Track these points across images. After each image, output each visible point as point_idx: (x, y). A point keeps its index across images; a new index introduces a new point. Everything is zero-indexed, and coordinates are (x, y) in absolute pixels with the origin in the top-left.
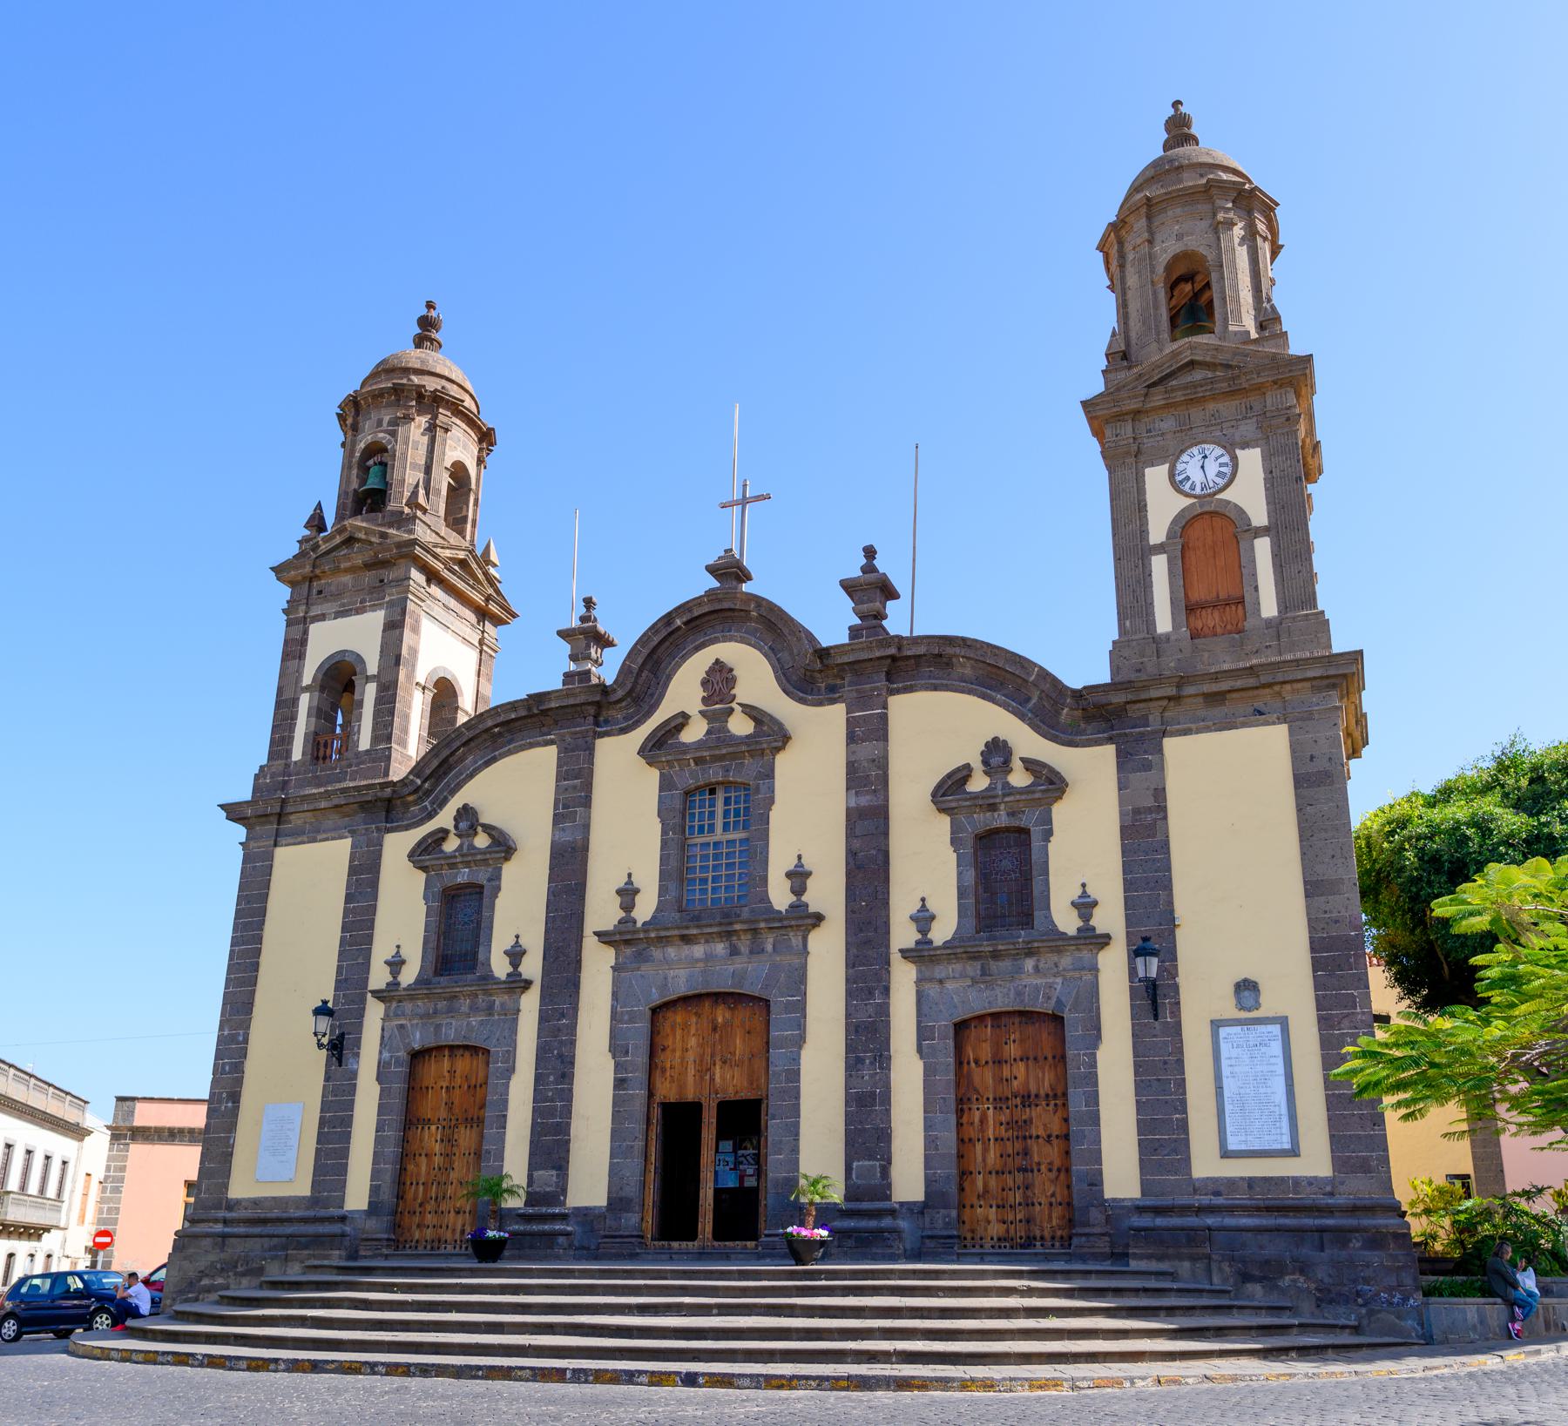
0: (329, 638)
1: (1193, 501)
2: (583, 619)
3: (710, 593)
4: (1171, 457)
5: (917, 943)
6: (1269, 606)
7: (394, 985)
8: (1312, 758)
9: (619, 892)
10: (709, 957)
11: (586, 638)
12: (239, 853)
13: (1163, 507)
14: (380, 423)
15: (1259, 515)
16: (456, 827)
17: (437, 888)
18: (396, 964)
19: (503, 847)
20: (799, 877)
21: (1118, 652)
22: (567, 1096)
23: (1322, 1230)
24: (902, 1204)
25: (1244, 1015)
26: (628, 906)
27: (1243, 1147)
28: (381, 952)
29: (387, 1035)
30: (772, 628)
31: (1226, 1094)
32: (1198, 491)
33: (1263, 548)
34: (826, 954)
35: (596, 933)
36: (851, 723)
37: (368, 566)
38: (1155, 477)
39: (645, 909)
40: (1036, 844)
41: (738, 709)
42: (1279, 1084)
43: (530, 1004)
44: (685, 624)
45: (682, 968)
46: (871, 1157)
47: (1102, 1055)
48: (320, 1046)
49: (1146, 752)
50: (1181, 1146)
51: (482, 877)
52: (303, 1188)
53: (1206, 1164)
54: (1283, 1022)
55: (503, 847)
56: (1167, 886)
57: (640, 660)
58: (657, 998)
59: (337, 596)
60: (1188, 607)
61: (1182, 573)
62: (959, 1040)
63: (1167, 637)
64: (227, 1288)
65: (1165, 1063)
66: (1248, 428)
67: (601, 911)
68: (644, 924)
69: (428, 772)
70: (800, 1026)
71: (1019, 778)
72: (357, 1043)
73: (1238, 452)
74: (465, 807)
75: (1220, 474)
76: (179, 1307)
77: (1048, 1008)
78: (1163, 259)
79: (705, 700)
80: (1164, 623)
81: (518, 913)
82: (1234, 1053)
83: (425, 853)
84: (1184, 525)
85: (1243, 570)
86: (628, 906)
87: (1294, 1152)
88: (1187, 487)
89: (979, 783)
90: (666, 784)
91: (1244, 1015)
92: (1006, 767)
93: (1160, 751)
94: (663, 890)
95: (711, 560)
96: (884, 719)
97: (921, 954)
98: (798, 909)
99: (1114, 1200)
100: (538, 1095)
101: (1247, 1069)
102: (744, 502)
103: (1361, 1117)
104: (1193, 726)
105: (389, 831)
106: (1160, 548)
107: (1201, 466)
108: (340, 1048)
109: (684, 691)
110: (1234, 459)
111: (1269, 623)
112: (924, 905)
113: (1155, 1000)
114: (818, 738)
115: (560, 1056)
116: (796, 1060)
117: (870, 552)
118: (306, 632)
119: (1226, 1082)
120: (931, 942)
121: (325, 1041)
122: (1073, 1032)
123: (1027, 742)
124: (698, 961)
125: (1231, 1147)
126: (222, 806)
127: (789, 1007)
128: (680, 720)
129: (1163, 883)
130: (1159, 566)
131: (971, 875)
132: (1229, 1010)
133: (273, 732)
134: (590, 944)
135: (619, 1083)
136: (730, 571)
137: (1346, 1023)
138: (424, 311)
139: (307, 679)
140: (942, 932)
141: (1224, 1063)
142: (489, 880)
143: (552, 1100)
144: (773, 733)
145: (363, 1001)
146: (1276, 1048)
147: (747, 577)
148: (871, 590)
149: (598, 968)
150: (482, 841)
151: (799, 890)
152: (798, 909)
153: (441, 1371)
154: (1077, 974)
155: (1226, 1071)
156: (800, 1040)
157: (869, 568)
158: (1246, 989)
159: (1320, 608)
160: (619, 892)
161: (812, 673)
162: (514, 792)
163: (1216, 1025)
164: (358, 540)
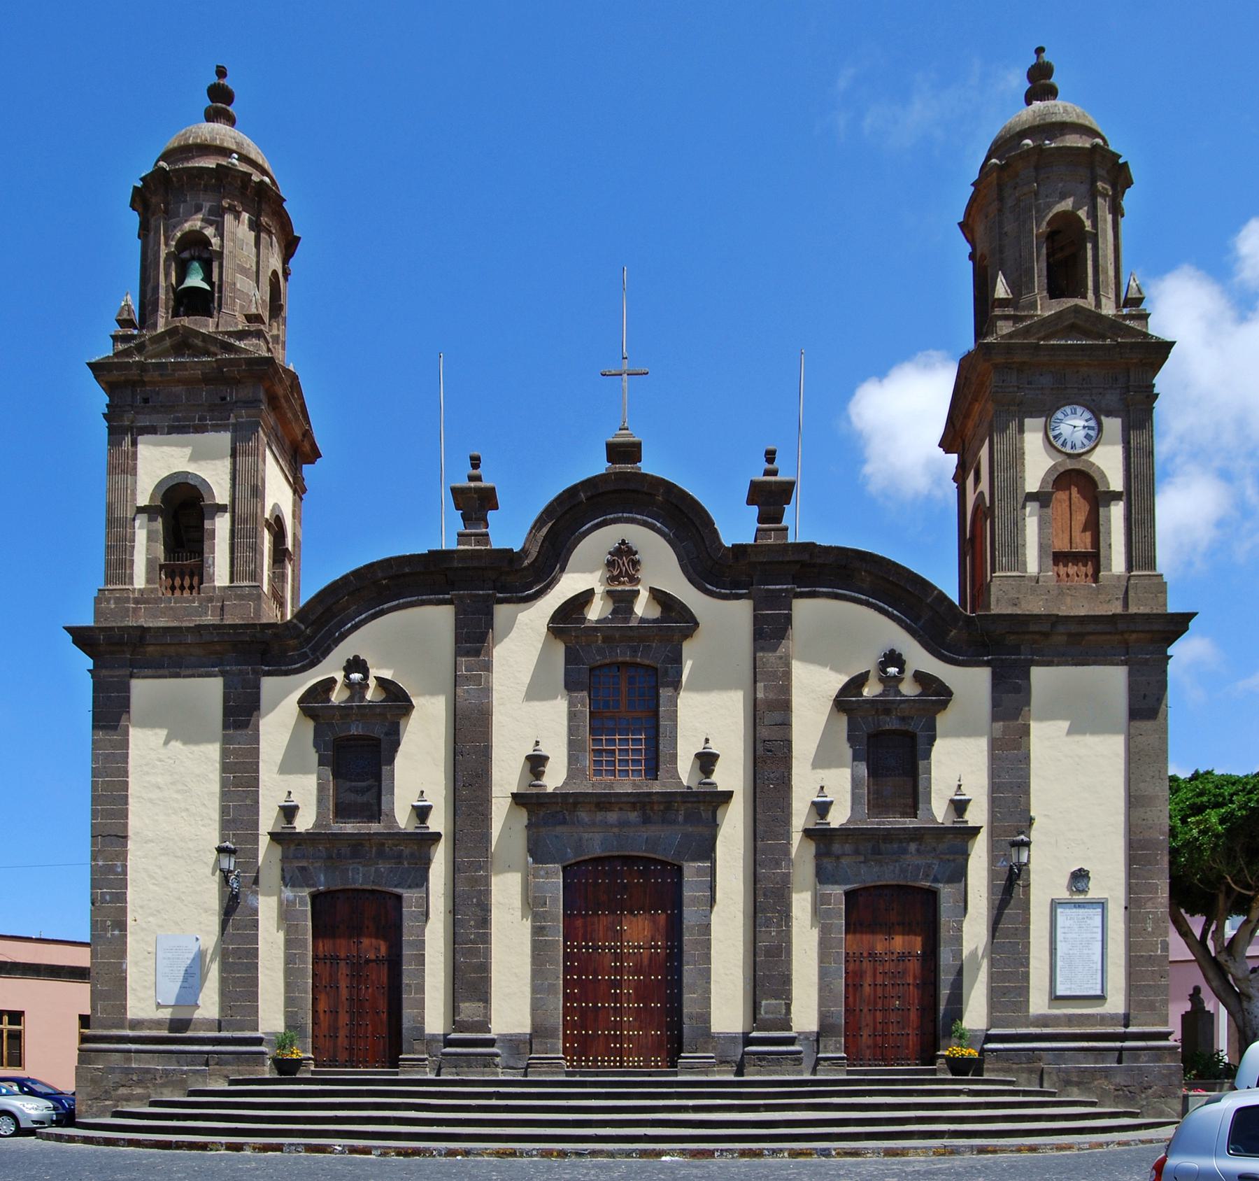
8: (1145, 696)
10: (622, 824)
15: (1116, 482)
17: (329, 738)
19: (397, 702)
23: (1121, 1050)
30: (682, 518)
33: (1117, 512)
51: (378, 731)
54: (1102, 904)
56: (1027, 792)
66: (1112, 398)
67: (506, 776)
71: (908, 689)
73: (1103, 418)
75: (1087, 437)
81: (418, 773)
82: (1068, 923)
88: (1058, 444)
93: (1028, 677)
103: (1153, 972)
104: (1055, 659)
107: (1073, 424)
109: (580, 578)
110: (1100, 424)
113: (1011, 885)
115: (478, 905)
119: (1059, 946)
123: (919, 658)
124: (612, 826)
125: (1059, 993)
129: (1024, 787)
131: (922, 764)
132: (1064, 894)
137: (1149, 904)
138: (214, 79)
142: (387, 734)
146: (1099, 918)
148: (770, 498)
153: (179, 1146)
154: (951, 857)
158: (1080, 877)
159: (1159, 570)
161: (713, 566)
163: (1055, 905)
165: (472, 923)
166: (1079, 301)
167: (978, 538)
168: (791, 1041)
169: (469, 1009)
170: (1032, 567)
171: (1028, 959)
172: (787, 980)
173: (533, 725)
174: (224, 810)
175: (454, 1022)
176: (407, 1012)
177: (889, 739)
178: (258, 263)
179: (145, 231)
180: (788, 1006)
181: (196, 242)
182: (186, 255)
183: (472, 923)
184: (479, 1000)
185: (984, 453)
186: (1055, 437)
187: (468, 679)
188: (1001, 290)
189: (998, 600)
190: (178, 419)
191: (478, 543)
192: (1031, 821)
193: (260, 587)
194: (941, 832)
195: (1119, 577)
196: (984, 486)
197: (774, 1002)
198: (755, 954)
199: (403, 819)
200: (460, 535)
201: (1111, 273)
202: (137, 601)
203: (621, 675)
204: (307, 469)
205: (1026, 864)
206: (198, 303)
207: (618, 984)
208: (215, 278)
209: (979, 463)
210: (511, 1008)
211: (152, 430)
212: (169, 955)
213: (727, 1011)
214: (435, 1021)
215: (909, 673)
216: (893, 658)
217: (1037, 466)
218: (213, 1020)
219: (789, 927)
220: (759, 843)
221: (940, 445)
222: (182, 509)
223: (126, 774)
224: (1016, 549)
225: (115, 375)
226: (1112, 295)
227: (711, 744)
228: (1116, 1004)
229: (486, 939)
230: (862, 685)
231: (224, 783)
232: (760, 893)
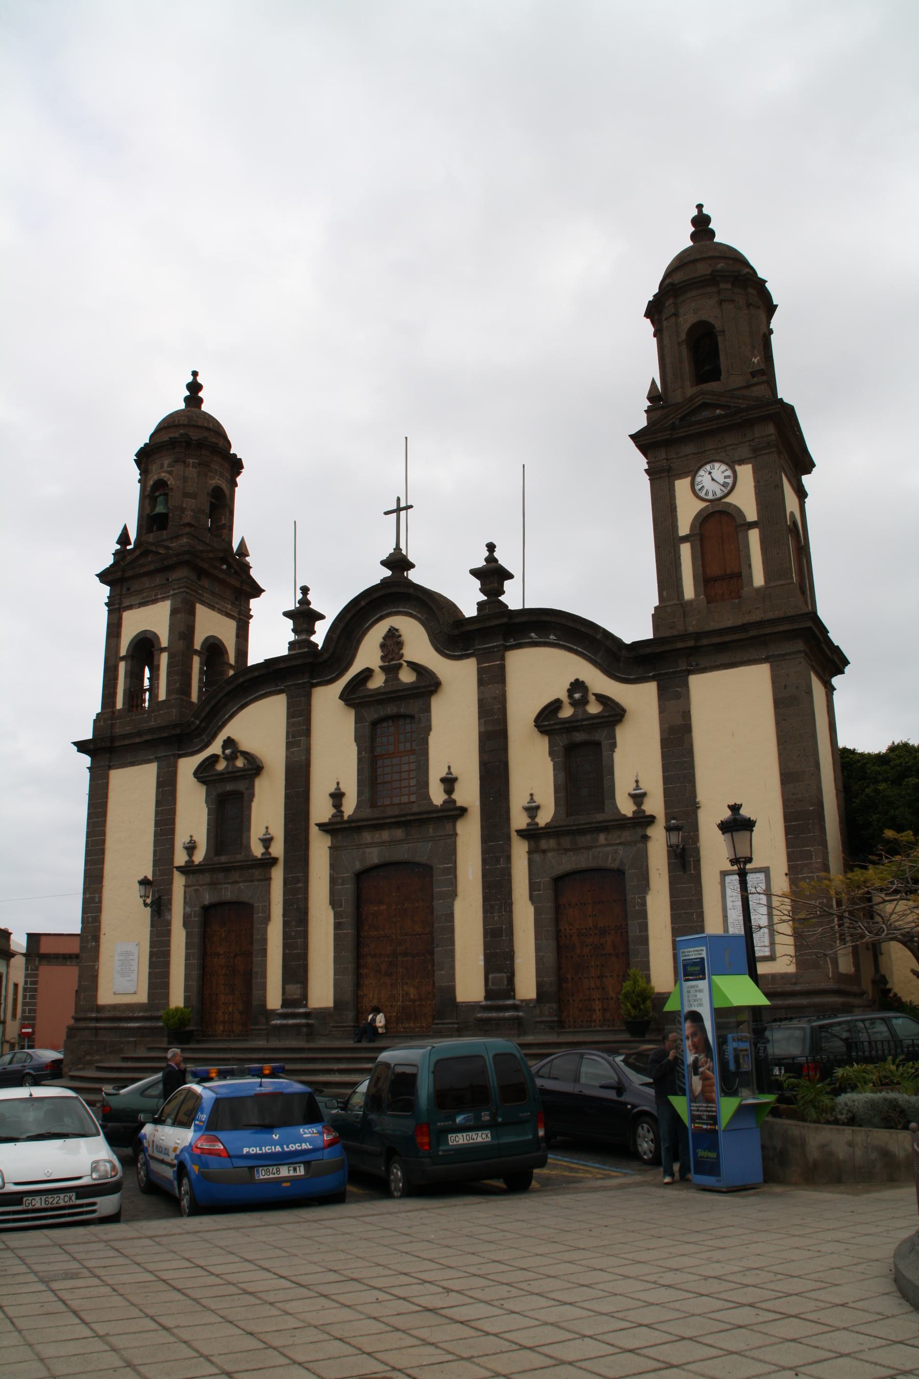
0: (136, 622)
1: (706, 504)
3: (385, 582)
4: (693, 473)
5: (528, 825)
7: (190, 862)
8: (785, 686)
9: (332, 795)
11: (304, 617)
12: (87, 775)
13: (687, 509)
15: (751, 514)
16: (223, 752)
18: (191, 848)
19: (255, 768)
20: (449, 783)
21: (658, 617)
22: (305, 935)
24: (522, 1001)
28: (181, 839)
29: (188, 897)
30: (431, 607)
31: (730, 920)
32: (710, 497)
33: (754, 536)
34: (469, 838)
35: (317, 825)
36: (480, 672)
37: (158, 571)
38: (682, 486)
39: (349, 806)
41: (405, 664)
43: (277, 875)
44: (368, 604)
45: (373, 850)
46: (501, 971)
47: (650, 899)
48: (146, 905)
52: (142, 997)
54: (766, 871)
55: (255, 768)
57: (338, 632)
58: (358, 866)
59: (139, 592)
60: (704, 580)
61: (700, 559)
62: (555, 893)
63: (690, 602)
64: (101, 1061)
65: (690, 901)
67: (321, 810)
68: (349, 816)
69: (203, 715)
70: (453, 883)
72: (170, 901)
74: (229, 738)
76: (71, 1074)
77: (615, 865)
78: (686, 327)
79: (383, 658)
80: (689, 592)
81: (267, 813)
83: (204, 774)
84: (703, 520)
89: (567, 712)
90: (358, 720)
92: (584, 701)
94: (360, 793)
95: (384, 557)
96: (502, 668)
97: (531, 834)
98: (450, 802)
100: (286, 936)
102: (398, 510)
105: (181, 756)
106: (685, 539)
107: (713, 477)
108: (159, 907)
109: (368, 654)
110: (735, 473)
111: (758, 590)
112: (532, 799)
114: (459, 678)
116: (451, 907)
117: (491, 547)
119: (729, 912)
120: (537, 824)
121: (149, 901)
122: (631, 883)
123: (599, 682)
126: (75, 744)
128: (366, 674)
129: (690, 779)
130: (686, 550)
134: (314, 831)
136: (398, 563)
139: (123, 652)
140: (545, 817)
142: (247, 789)
144: (428, 684)
145: (172, 874)
147: (248, 555)
148: (492, 576)
150: (240, 763)
152: (450, 802)
156: (453, 894)
157: (491, 559)
160: (332, 795)
164: (151, 552)
165: (294, 923)
168: (515, 1007)
176: (256, 993)
183: (294, 923)
194: (623, 823)
197: (498, 975)
199: (257, 850)
204: (805, 479)
210: (322, 992)
213: (470, 984)
214: (274, 1000)
216: (577, 686)
225: (110, 578)
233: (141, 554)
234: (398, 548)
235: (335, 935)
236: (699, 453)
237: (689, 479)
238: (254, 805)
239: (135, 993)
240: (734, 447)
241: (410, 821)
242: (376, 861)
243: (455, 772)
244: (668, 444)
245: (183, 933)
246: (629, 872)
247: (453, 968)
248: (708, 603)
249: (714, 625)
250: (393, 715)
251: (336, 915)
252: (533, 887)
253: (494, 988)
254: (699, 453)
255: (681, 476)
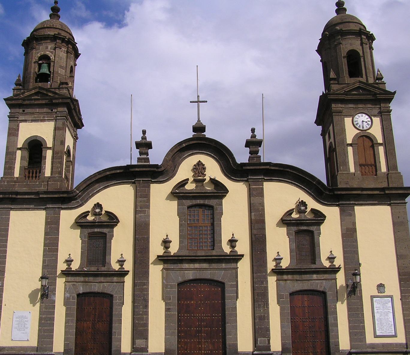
0: (28, 130)
1: (359, 131)
2: (143, 138)
6: (384, 169)
14: (47, 48)
15: (380, 140)
19: (112, 220)
20: (232, 242)
25: (380, 294)
26: (167, 248)
27: (381, 334)
31: (376, 318)
33: (381, 149)
34: (244, 268)
40: (316, 237)
42: (391, 315)
43: (128, 280)
44: (186, 146)
45: (190, 272)
49: (350, 211)
50: (363, 333)
52: (33, 342)
53: (370, 339)
54: (391, 297)
56: (357, 253)
58: (180, 280)
60: (360, 165)
62: (293, 301)
65: (358, 308)
67: (156, 249)
69: (82, 188)
73: (373, 118)
79: (194, 176)
81: (121, 246)
82: (378, 306)
85: (375, 156)
86: (167, 248)
87: (395, 336)
88: (357, 127)
91: (380, 294)
97: (278, 272)
99: (342, 350)
101: (382, 311)
107: (362, 119)
109: (185, 171)
114: (237, 192)
117: (144, 132)
118: (18, 126)
123: (312, 204)
125: (377, 334)
127: (232, 286)
131: (294, 245)
132: (376, 293)
133: (5, 165)
135: (167, 310)
136: (199, 129)
138: (54, 5)
141: (375, 309)
142: (109, 232)
143: (142, 315)
144: (220, 191)
146: (390, 304)
149: (156, 273)
151: (233, 247)
155: (375, 311)
157: (144, 138)
158: (381, 287)
161: (234, 171)
162: (118, 199)
163: (372, 297)
165: (141, 307)
166: (360, 79)
167: (332, 156)
169: (140, 343)
170: (352, 169)
171: (364, 320)
172: (268, 330)
173: (166, 221)
174: (44, 261)
175: (133, 348)
177: (303, 229)
178: (66, 64)
179: (26, 54)
180: (269, 341)
181: (45, 58)
182: (40, 62)
183: (141, 307)
184: (144, 339)
185: (331, 128)
186: (356, 124)
187: (141, 212)
188: (332, 75)
189: (340, 182)
190: (35, 117)
191: (145, 162)
192: (360, 264)
193: (62, 177)
195: (384, 173)
196: (332, 140)
197: (263, 339)
198: (254, 319)
200: (138, 159)
201: (371, 69)
202: (15, 182)
203: (200, 204)
205: (359, 282)
206: (44, 78)
207: (200, 332)
208: (52, 70)
209: (329, 131)
211: (25, 121)
212: (18, 320)
215: (308, 210)
217: (351, 133)
218: (34, 347)
219: (268, 308)
220: (255, 275)
221: (315, 123)
222: (35, 147)
223: (6, 247)
224: (346, 163)
225: (10, 102)
226: (372, 76)
227: (234, 236)
228: (401, 339)
229: (147, 313)
230: (291, 213)
231: (45, 251)
232: (256, 294)
233: (35, 93)
234: (199, 121)
235: (166, 314)
236: (355, 108)
237: (351, 118)
238: (113, 241)
239: (28, 340)
240: (371, 108)
241: (182, 260)
242: (191, 278)
243: (236, 237)
244: (19, 106)
245: (162, 305)
246: (329, 294)
247: (236, 334)
248: (362, 175)
249: (365, 186)
250: (200, 204)
251: (166, 304)
252: (279, 297)
253: (261, 345)
254: (355, 108)
255: (348, 116)
